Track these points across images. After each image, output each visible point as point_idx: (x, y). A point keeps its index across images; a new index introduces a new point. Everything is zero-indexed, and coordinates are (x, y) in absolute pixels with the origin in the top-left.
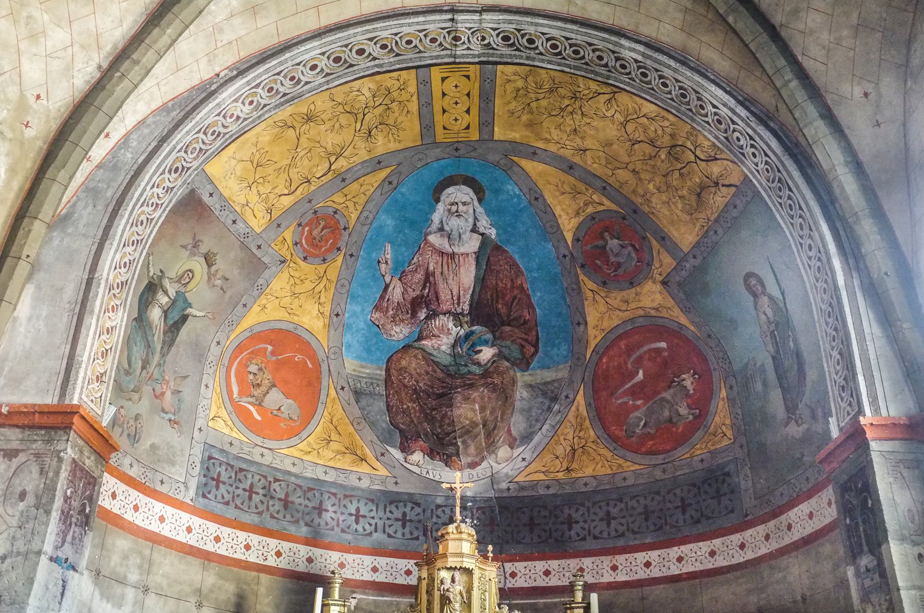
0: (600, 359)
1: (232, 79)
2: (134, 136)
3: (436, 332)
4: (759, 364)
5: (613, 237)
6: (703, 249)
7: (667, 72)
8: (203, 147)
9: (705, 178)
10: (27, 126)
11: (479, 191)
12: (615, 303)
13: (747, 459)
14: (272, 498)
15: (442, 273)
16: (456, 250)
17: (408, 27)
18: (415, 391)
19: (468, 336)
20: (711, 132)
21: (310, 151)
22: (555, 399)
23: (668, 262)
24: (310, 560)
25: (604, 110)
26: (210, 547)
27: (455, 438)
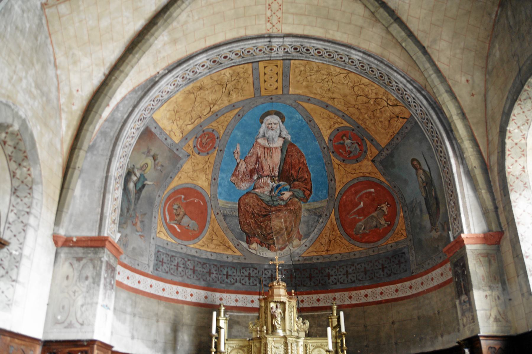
0: (342, 197)
1: (165, 75)
2: (121, 105)
3: (262, 185)
4: (418, 202)
5: (348, 139)
6: (391, 146)
7: (373, 66)
8: (153, 107)
9: (392, 114)
10: (73, 105)
11: (282, 118)
12: (349, 170)
13: (413, 246)
14: (187, 268)
15: (265, 157)
16: (271, 146)
17: (248, 45)
18: (253, 214)
19: (277, 187)
20: (395, 94)
21: (201, 103)
22: (320, 216)
23: (375, 152)
24: (206, 297)
25: (343, 81)
26: (161, 294)
27: (273, 236)
